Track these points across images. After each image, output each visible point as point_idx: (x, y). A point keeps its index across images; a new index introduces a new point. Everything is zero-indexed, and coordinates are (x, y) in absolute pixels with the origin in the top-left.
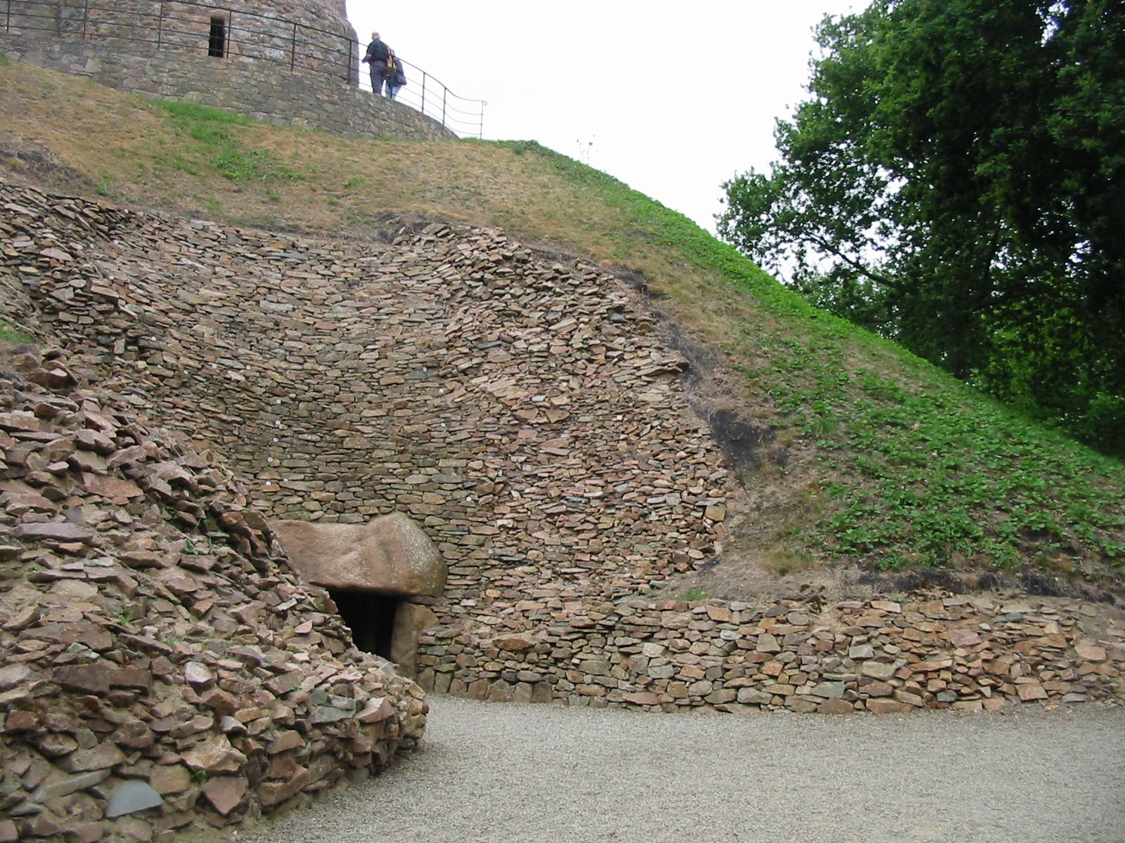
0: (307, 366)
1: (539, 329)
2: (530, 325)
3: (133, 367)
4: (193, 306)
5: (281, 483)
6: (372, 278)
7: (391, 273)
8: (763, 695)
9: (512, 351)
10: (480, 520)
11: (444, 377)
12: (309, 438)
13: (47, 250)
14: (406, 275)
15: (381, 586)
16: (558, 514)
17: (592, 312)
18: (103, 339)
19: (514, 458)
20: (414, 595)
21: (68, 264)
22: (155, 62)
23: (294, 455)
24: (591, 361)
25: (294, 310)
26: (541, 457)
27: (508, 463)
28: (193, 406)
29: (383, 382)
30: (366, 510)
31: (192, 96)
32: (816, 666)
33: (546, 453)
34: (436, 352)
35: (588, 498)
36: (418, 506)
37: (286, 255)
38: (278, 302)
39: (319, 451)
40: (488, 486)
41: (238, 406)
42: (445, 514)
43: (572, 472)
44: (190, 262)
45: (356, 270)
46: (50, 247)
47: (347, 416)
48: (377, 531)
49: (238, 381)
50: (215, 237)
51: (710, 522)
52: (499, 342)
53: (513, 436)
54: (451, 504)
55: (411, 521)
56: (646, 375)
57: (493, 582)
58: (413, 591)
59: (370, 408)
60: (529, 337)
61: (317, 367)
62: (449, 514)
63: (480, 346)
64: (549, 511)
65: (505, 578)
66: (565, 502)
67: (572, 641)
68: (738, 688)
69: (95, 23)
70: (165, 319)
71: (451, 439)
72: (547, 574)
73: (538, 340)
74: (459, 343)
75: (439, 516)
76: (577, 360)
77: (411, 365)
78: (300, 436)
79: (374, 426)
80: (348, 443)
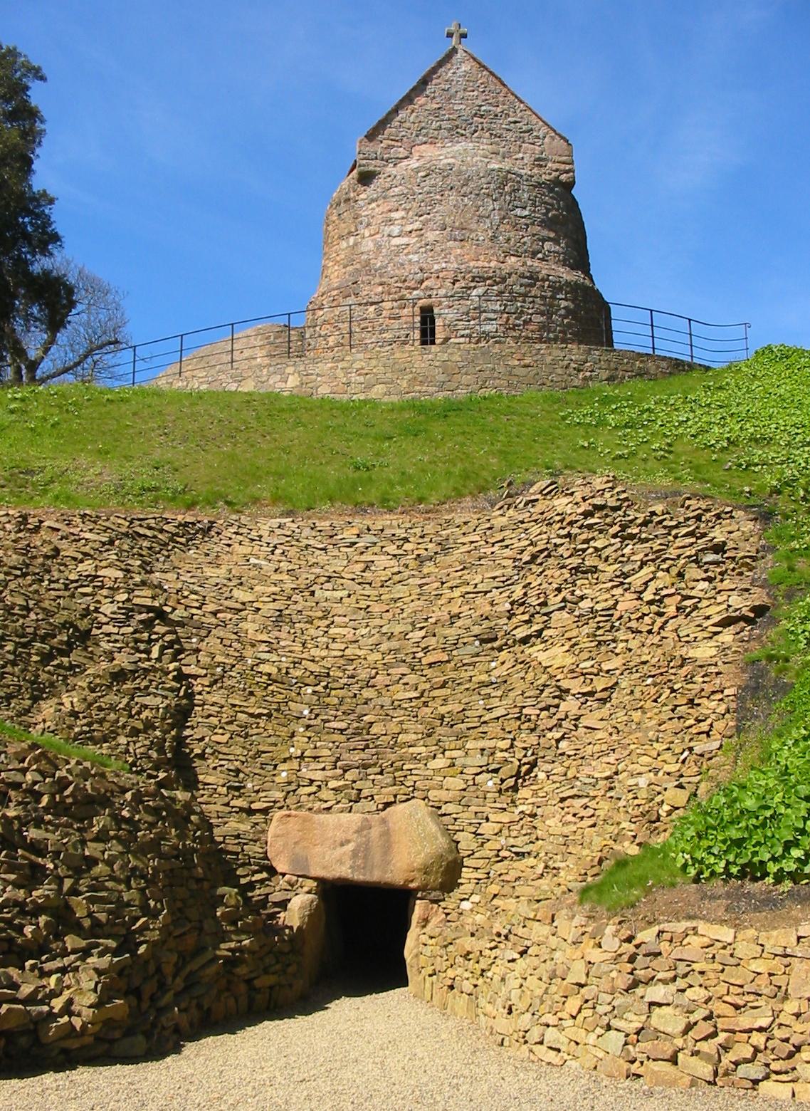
0: (348, 652)
4: (243, 604)
7: (473, 542)
9: (577, 613)
18: (142, 646)
19: (549, 735)
24: (660, 614)
28: (223, 702)
29: (424, 661)
30: (379, 799)
31: (380, 388)
37: (357, 540)
39: (343, 738)
40: (511, 768)
41: (267, 698)
43: (597, 748)
44: (256, 561)
45: (430, 546)
49: (269, 675)
50: (289, 533)
52: (563, 604)
53: (553, 710)
56: (713, 625)
58: (413, 885)
59: (405, 690)
63: (544, 610)
69: (326, 337)
73: (608, 596)
76: (645, 615)
78: (327, 725)
79: (406, 709)
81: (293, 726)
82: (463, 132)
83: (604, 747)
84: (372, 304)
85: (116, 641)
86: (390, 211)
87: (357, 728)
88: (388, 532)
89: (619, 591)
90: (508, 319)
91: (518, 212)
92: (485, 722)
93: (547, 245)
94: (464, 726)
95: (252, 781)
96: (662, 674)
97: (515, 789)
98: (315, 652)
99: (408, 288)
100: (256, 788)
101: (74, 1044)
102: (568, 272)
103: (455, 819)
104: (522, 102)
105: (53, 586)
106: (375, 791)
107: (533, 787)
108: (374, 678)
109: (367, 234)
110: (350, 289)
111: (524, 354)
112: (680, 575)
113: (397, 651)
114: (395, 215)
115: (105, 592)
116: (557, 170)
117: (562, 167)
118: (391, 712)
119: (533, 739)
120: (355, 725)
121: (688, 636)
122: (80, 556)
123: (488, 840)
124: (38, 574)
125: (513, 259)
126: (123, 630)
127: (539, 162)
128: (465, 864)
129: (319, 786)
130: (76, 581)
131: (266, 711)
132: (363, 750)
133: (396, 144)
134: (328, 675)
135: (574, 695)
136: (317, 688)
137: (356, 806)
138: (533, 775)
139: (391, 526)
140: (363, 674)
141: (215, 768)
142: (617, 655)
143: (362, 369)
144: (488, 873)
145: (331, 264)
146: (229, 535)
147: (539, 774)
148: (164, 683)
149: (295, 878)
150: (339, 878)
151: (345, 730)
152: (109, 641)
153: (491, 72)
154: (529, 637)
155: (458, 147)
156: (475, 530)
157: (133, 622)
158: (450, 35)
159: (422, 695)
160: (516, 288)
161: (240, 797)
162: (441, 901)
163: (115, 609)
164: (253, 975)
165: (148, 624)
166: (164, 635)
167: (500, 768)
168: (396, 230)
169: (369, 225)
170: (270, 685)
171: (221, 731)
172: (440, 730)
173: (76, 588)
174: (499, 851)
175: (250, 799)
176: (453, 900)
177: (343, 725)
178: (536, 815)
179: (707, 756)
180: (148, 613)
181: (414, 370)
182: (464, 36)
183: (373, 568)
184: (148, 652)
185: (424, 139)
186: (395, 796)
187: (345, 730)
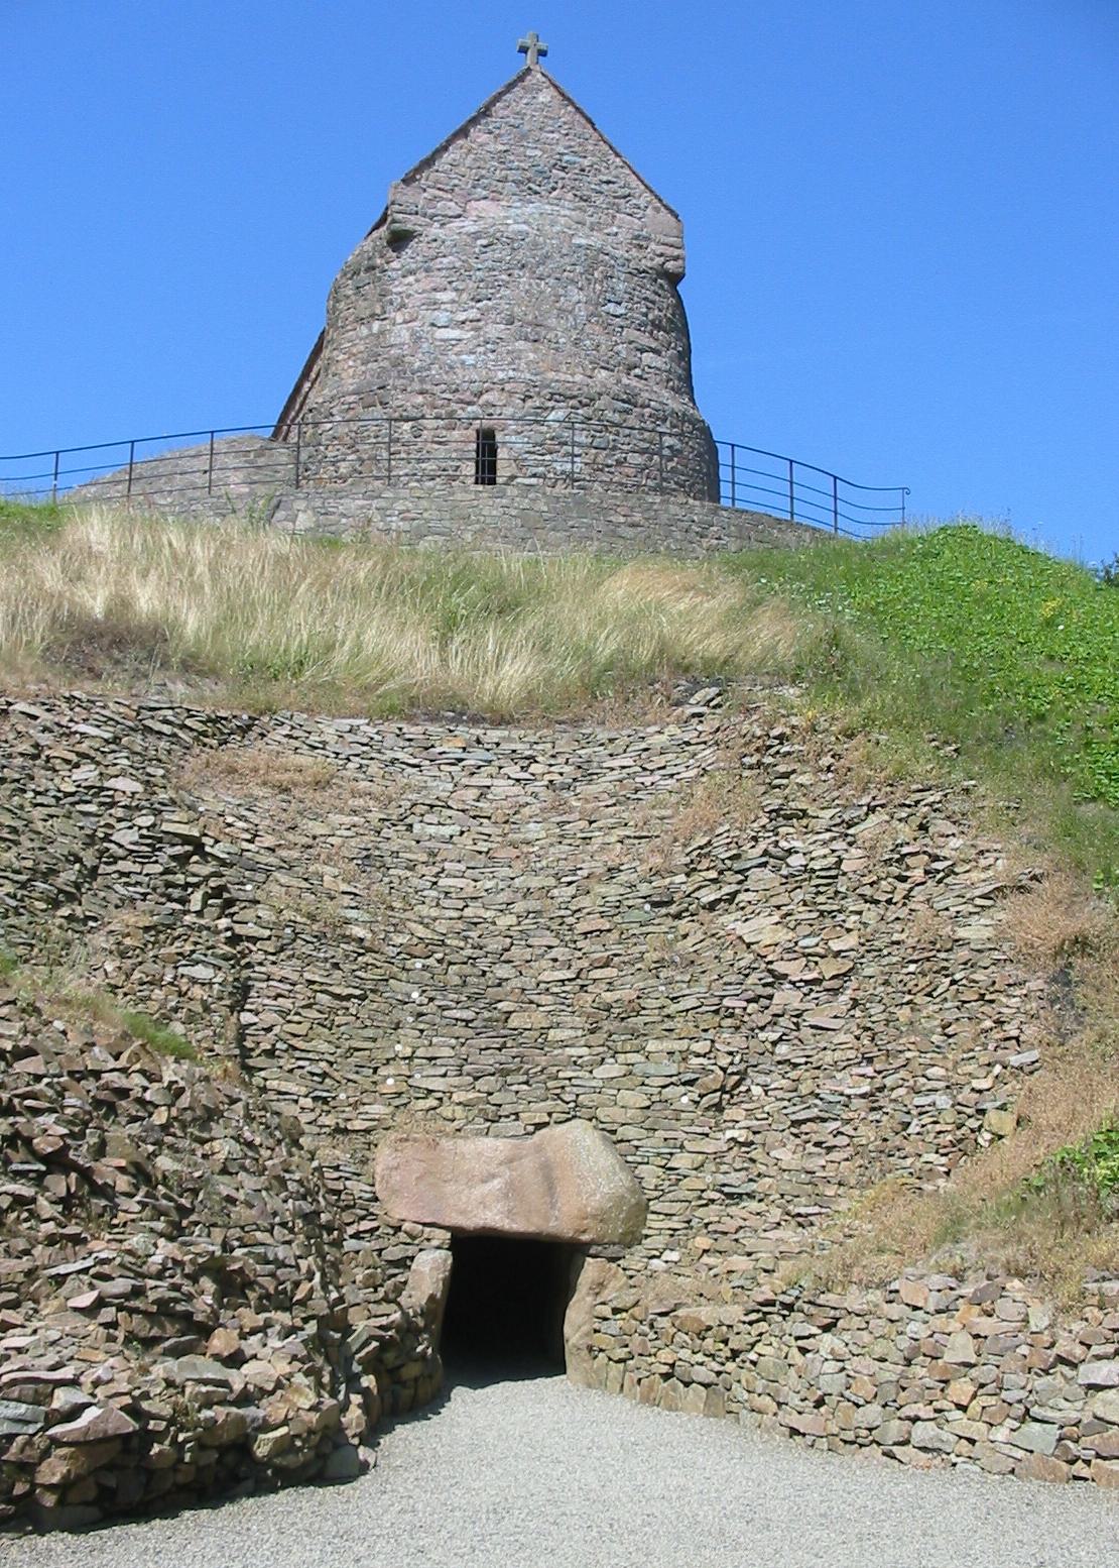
0: (468, 912)
1: (827, 836)
2: (817, 829)
3: (208, 929)
5: (410, 1081)
6: (590, 777)
7: (624, 767)
8: (945, 1436)
9: (784, 872)
10: (699, 1130)
11: (678, 916)
12: (458, 1016)
13: (113, 780)
14: (645, 769)
15: (532, 1229)
16: (804, 1122)
17: (917, 802)
18: (176, 893)
19: (762, 1036)
20: (589, 1244)
21: (137, 796)
22: (382, 503)
23: (435, 1040)
24: (903, 879)
25: (462, 833)
26: (806, 1032)
27: (752, 1043)
28: (295, 977)
30: (530, 1118)
32: (1023, 1394)
33: (812, 1027)
34: (668, 880)
35: (849, 1096)
37: (464, 756)
38: (440, 824)
39: (471, 1032)
40: (714, 1080)
41: (358, 973)
42: (646, 1125)
43: (838, 1055)
45: (567, 769)
46: (117, 776)
47: (516, 983)
48: (539, 1149)
49: (362, 940)
50: (365, 740)
51: (988, 1136)
52: (764, 859)
54: (658, 1106)
55: (597, 1134)
56: (980, 897)
57: (707, 1225)
58: (585, 1238)
60: (812, 848)
61: (482, 912)
62: (655, 1123)
63: (737, 866)
64: (794, 1117)
65: (723, 1219)
66: (817, 1102)
67: (751, 1323)
68: (915, 1419)
70: (272, 860)
71: (673, 1008)
72: (776, 1214)
73: (826, 851)
74: (705, 863)
75: (640, 1125)
77: (626, 903)
78: (446, 1013)
80: (515, 1021)
81: (397, 1014)
82: (537, 188)
83: (851, 1054)
84: (407, 420)
85: (138, 883)
86: (435, 290)
87: (489, 1019)
88: (506, 747)
89: (840, 845)
90: (596, 456)
91: (611, 307)
92: (668, 1016)
93: (647, 357)
95: (346, 1091)
96: (928, 959)
97: (719, 1108)
98: (424, 910)
99: (461, 401)
100: (351, 1100)
101: (290, 1461)
102: (674, 398)
103: (637, 1147)
104: (617, 155)
105: (39, 799)
107: (745, 1106)
108: (508, 950)
109: (399, 319)
110: (373, 395)
111: (632, 509)
112: (923, 827)
113: (538, 913)
114: (440, 296)
115: (119, 812)
116: (661, 255)
117: (670, 251)
118: (535, 998)
119: (738, 1041)
120: (486, 1014)
121: (947, 909)
122: (74, 758)
123: (685, 1177)
124: (18, 781)
125: (604, 373)
126: (148, 869)
127: (639, 242)
128: (652, 1208)
129: (440, 1099)
130: (72, 794)
131: (358, 992)
132: (500, 1049)
133: (445, 195)
135: (794, 983)
136: (428, 962)
138: (743, 1088)
139: (509, 739)
140: (494, 945)
141: (291, 1071)
142: (849, 931)
143: (408, 511)
144: (689, 1222)
145: (341, 357)
146: (278, 738)
147: (753, 1087)
148: (213, 947)
149: (420, 1227)
151: (472, 1021)
152: (127, 884)
153: (577, 109)
154: (719, 900)
155: (530, 208)
156: (625, 751)
157: (163, 857)
158: (524, 50)
160: (609, 414)
162: (619, 1259)
163: (136, 838)
165: (182, 860)
166: (207, 878)
167: (697, 1079)
168: (442, 317)
169: (403, 306)
170: (363, 954)
172: (606, 1026)
173: (73, 804)
174: (703, 1191)
175: (344, 1115)
177: (468, 1014)
178: (752, 1143)
179: (1027, 1069)
180: (182, 845)
181: (482, 519)
182: (542, 53)
183: (490, 796)
184: (183, 901)
185: (484, 193)
186: (550, 1114)
187: (472, 1021)
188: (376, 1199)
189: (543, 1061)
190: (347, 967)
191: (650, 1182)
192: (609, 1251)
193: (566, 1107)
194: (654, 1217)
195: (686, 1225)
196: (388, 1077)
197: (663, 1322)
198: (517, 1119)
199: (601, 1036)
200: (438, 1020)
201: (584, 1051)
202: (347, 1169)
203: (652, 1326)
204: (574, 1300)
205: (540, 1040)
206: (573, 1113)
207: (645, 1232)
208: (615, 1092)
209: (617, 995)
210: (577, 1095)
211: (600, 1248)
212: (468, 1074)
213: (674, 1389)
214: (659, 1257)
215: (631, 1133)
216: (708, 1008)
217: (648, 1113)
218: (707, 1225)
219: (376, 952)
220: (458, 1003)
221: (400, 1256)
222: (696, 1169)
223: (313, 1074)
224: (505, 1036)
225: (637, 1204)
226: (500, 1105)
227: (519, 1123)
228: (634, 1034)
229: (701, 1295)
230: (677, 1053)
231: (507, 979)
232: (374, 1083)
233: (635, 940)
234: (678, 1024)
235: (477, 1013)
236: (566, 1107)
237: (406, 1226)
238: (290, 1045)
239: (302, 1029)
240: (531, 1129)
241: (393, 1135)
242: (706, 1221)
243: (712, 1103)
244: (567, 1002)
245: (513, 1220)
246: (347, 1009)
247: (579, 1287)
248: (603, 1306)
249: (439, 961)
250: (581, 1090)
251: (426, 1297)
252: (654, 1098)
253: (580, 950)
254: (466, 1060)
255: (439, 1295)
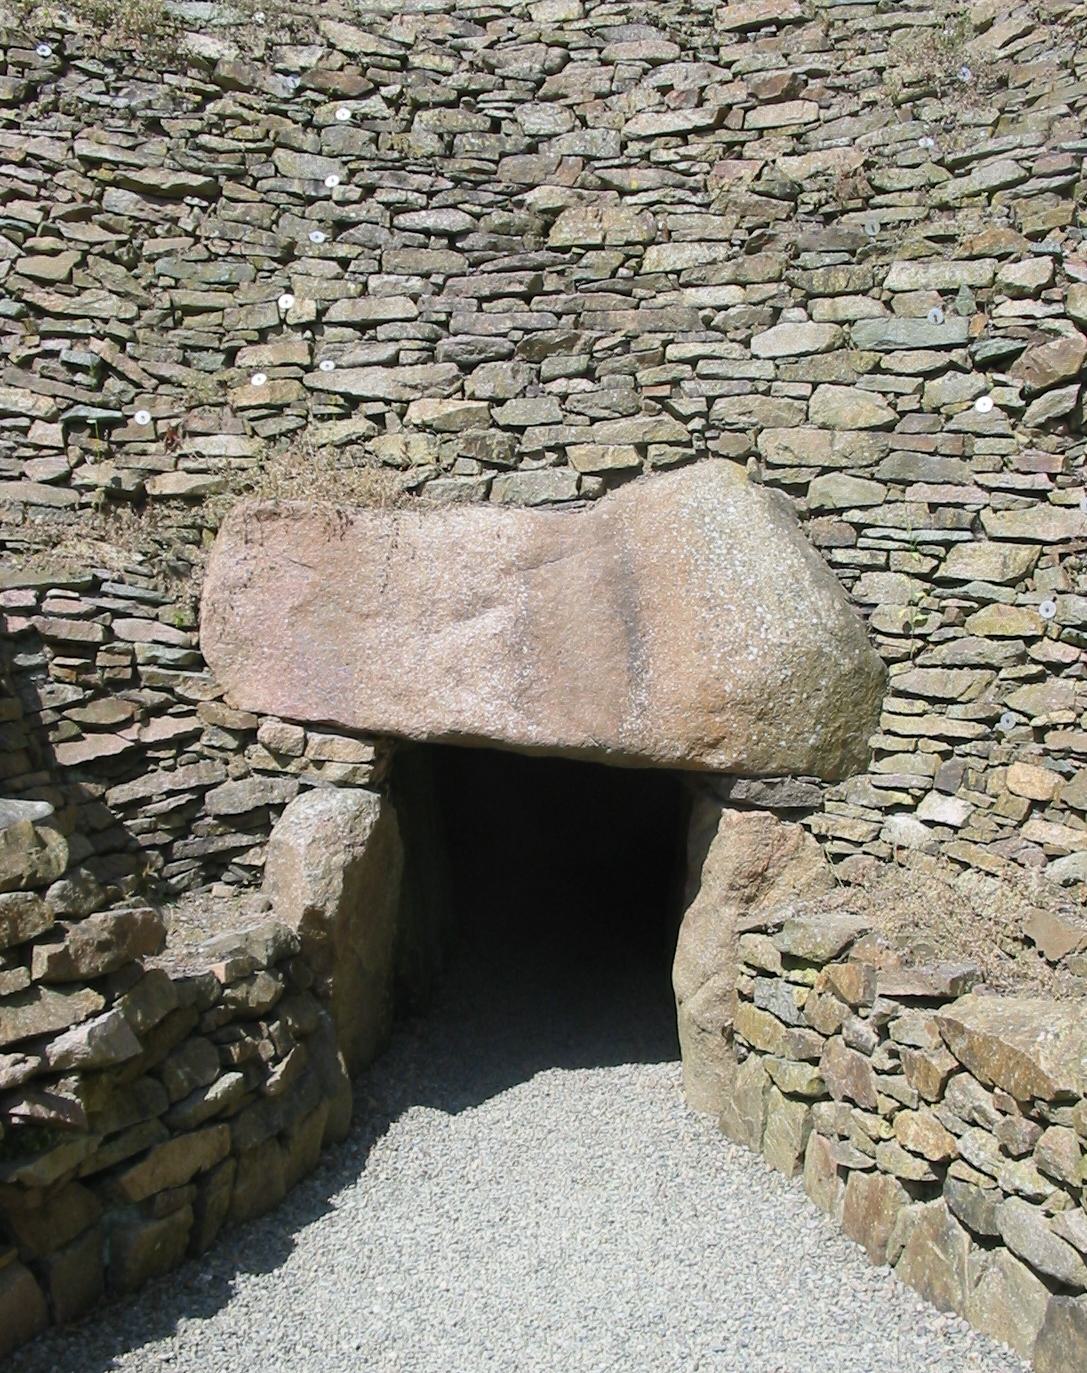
5: (310, 379)
15: (554, 740)
23: (374, 282)
28: (55, 153)
36: (785, 436)
39: (457, 261)
40: (1063, 352)
41: (204, 139)
42: (885, 470)
47: (573, 143)
49: (212, 63)
55: (758, 493)
57: (1040, 733)
58: (717, 759)
59: (663, 108)
62: (904, 464)
71: (953, 188)
75: (868, 471)
78: (402, 220)
79: (666, 165)
81: (290, 227)
87: (504, 229)
92: (944, 207)
94: (872, 218)
100: (162, 426)
103: (859, 527)
106: (568, 434)
118: (616, 176)
120: (497, 217)
123: (984, 602)
128: (895, 683)
129: (379, 419)
131: (198, 180)
132: (526, 298)
134: (404, 65)
137: (503, 483)
140: (523, 62)
141: (26, 363)
144: (991, 721)
149: (299, 731)
150: (454, 733)
159: (720, 123)
161: (109, 455)
164: (115, 1154)
167: (1018, 352)
171: (48, 242)
172: (785, 233)
175: (144, 463)
176: (852, 810)
187: (464, 234)
188: (198, 663)
189: (628, 320)
190: (178, 126)
191: (892, 615)
192: (785, 791)
193: (680, 431)
194: (900, 704)
195: (982, 729)
196: (258, 369)
197: (915, 1026)
198: (562, 462)
199: (771, 261)
200: (382, 235)
201: (733, 294)
202: (122, 590)
203: (883, 1032)
204: (695, 905)
205: (623, 272)
206: (698, 444)
207: (877, 741)
208: (806, 390)
209: (814, 162)
210: (711, 401)
211: (757, 786)
212: (449, 358)
213: (943, 1238)
214: (910, 809)
215: (845, 491)
216: (1045, 183)
217: (891, 440)
218: (1040, 733)
219: (246, 90)
220: (431, 195)
221: (249, 806)
222: (1011, 583)
223: (74, 368)
224: (540, 267)
225: (858, 671)
226: (521, 429)
227: (567, 471)
228: (857, 251)
229: (1028, 942)
230: (965, 292)
231: (550, 137)
232: (223, 384)
233: (861, 43)
234: (967, 223)
235: (477, 217)
236: (680, 431)
237: (267, 730)
238: (30, 305)
239: (56, 268)
240: (592, 483)
241: (248, 503)
242: (1037, 722)
243: (1054, 413)
244: (691, 181)
245: (529, 714)
246: (175, 220)
247: (707, 879)
248: (759, 937)
249: (390, 102)
250: (719, 388)
251: (300, 913)
252: (904, 404)
253: (728, 65)
254: (445, 325)
255: (331, 909)
